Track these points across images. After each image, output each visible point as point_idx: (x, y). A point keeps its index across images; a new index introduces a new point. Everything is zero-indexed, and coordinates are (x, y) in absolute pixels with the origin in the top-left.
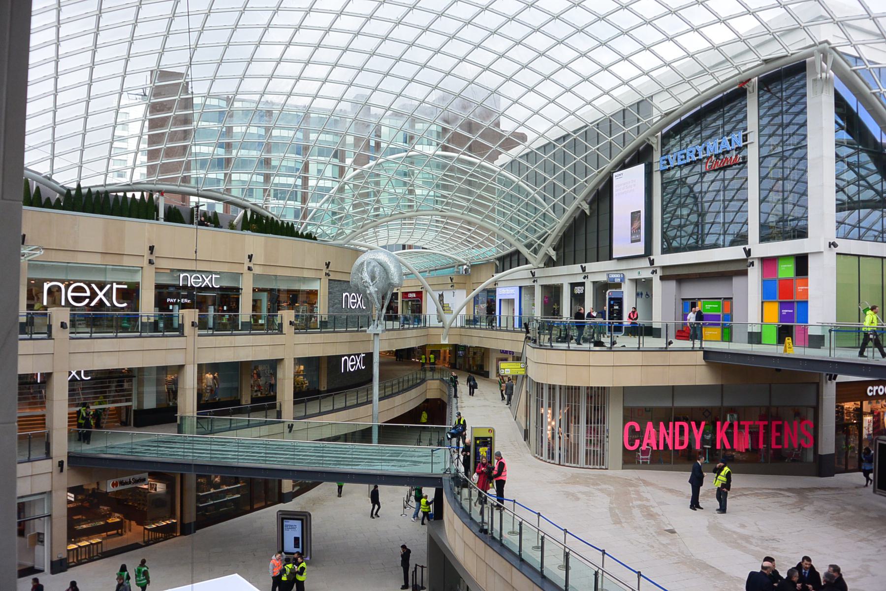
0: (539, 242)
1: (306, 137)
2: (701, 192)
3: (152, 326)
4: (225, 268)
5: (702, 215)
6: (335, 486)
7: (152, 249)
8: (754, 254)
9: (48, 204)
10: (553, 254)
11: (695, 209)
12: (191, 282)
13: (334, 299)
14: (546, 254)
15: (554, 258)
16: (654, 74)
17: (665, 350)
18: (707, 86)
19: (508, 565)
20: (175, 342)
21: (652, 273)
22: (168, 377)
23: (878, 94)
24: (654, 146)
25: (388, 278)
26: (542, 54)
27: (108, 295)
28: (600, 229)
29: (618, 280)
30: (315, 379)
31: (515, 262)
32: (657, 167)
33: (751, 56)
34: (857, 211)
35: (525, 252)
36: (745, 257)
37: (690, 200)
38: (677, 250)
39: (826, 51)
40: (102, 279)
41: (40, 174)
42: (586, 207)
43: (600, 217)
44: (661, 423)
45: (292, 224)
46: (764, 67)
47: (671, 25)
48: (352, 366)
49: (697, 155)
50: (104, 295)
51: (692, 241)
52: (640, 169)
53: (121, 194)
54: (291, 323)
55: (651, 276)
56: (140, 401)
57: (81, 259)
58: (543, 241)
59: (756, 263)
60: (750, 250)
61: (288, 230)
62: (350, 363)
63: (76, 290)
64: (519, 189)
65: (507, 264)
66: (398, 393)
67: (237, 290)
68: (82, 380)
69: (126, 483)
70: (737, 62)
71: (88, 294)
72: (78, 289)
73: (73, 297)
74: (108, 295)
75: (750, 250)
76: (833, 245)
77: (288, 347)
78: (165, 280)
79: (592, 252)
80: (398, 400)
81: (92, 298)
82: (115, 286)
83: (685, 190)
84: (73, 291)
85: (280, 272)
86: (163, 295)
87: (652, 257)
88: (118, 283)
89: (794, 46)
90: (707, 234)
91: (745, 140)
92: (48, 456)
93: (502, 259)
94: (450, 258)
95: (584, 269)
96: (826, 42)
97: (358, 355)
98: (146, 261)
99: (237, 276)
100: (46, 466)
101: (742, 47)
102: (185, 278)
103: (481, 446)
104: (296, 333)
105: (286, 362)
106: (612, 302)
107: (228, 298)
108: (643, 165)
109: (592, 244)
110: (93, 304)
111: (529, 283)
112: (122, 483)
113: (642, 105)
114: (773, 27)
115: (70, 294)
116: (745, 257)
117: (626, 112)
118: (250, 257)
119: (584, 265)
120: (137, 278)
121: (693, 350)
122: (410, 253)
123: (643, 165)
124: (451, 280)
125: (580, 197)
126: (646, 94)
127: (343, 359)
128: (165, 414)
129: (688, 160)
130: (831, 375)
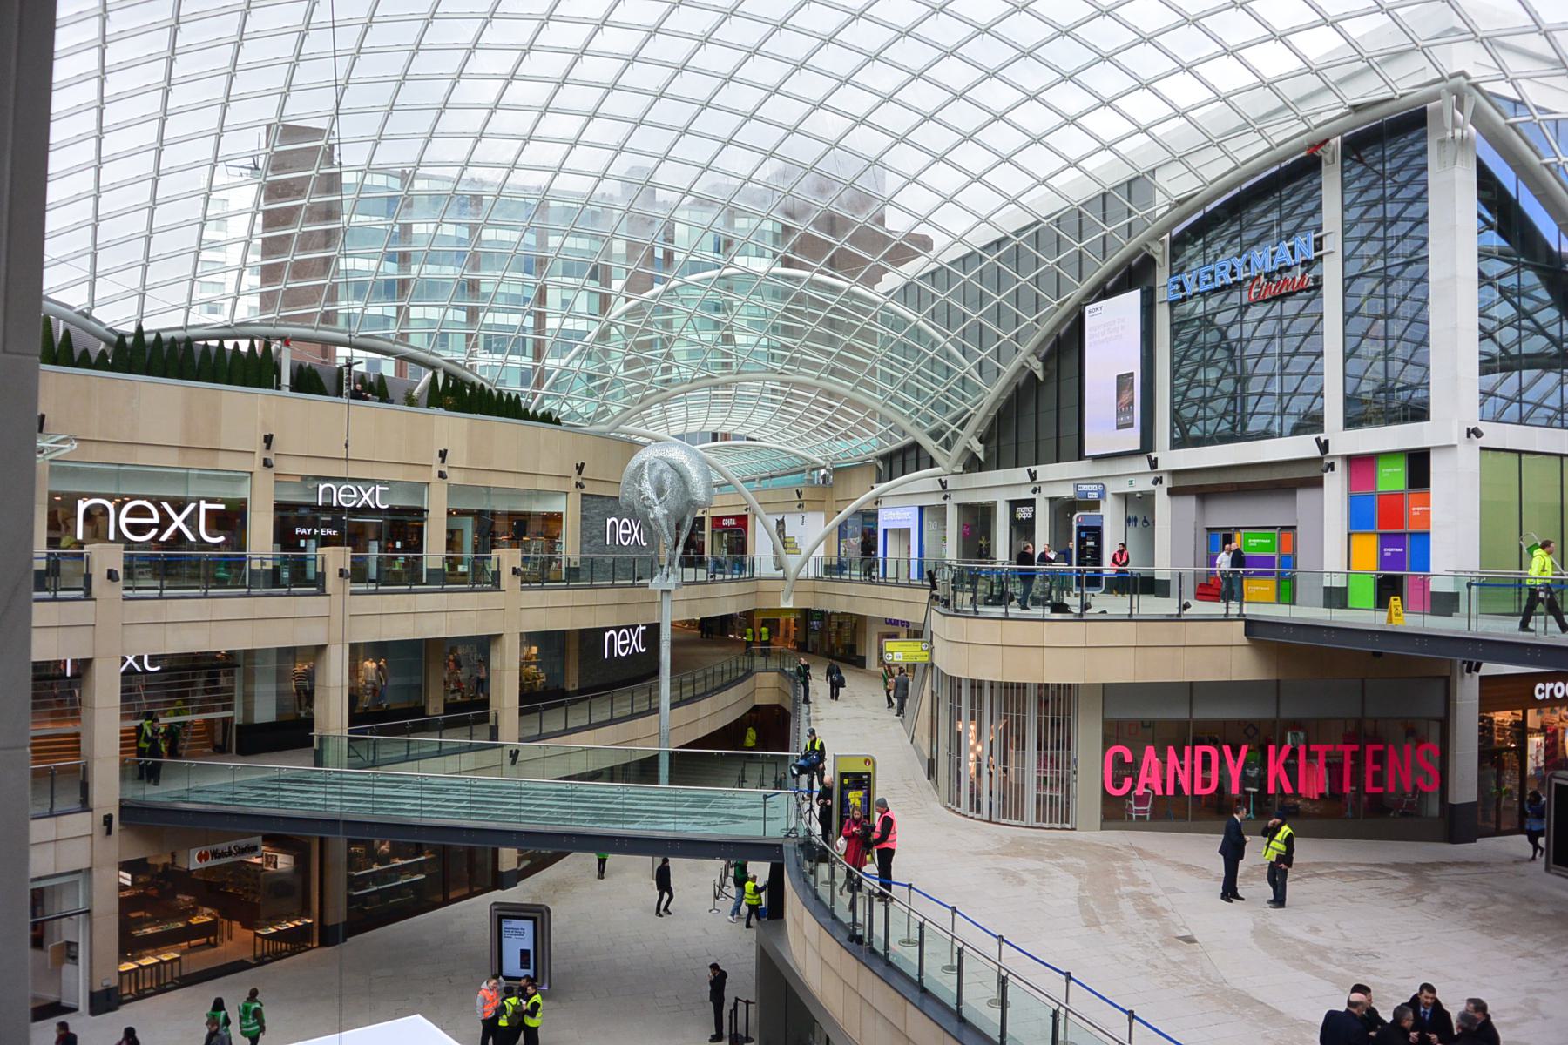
0: (953, 428)
1: (542, 242)
2: (1240, 340)
3: (270, 577)
4: (398, 474)
5: (1242, 380)
6: (592, 859)
7: (268, 439)
8: (1334, 450)
9: (84, 361)
10: (979, 449)
11: (1230, 369)
12: (339, 498)
13: (591, 528)
14: (966, 449)
15: (981, 456)
16: (1157, 131)
17: (1177, 618)
18: (1251, 152)
19: (900, 999)
20: (309, 605)
21: (1155, 483)
22: (297, 667)
23: (1554, 167)
24: (1157, 258)
25: (686, 491)
26: (959, 96)
27: (191, 521)
28: (1062, 404)
29: (1093, 496)
30: (557, 670)
31: (911, 463)
32: (1162, 295)
33: (1329, 100)
34: (1516, 373)
35: (929, 445)
36: (1318, 454)
37: (1220, 354)
38: (1198, 442)
39: (1461, 90)
40: (180, 493)
41: (71, 308)
42: (1037, 366)
43: (1062, 384)
44: (1171, 748)
45: (518, 397)
46: (1352, 119)
47: (1188, 44)
48: (623, 647)
49: (1233, 274)
50: (185, 522)
51: (1224, 426)
52: (1133, 298)
53: (215, 343)
54: (515, 571)
55: (1153, 487)
56: (248, 709)
57: (144, 457)
58: (962, 427)
59: (1338, 465)
60: (1327, 442)
61: (509, 408)
62: (619, 643)
63: (134, 512)
64: (918, 334)
65: (898, 466)
66: (705, 695)
67: (420, 513)
68: (145, 672)
69: (223, 855)
70: (1304, 109)
71: (156, 519)
72: (138, 511)
73: (129, 526)
74: (191, 521)
75: (1327, 442)
76: (1474, 433)
77: (510, 614)
78: (292, 495)
79: (1048, 446)
80: (705, 707)
81: (162, 527)
82: (204, 506)
83: (1213, 337)
84: (129, 515)
85: (495, 481)
86: (288, 521)
87: (1153, 455)
88: (209, 501)
89: (1405, 82)
90: (1252, 414)
91: (1318, 247)
92: (85, 806)
93: (888, 458)
94: (797, 456)
95: (1033, 476)
96: (1463, 73)
97: (634, 627)
98: (258, 462)
99: (419, 488)
100: (81, 823)
101: (1313, 83)
102: (328, 492)
103: (852, 789)
104: (523, 589)
105: (507, 640)
106: (1083, 535)
107: (403, 526)
108: (1138, 292)
109: (1048, 432)
110: (164, 538)
111: (936, 500)
112: (216, 855)
113: (1137, 186)
114: (1369, 48)
115: (124, 520)
116: (1318, 454)
117: (1108, 198)
118: (443, 455)
119: (1033, 468)
120: (243, 492)
121: (1226, 618)
122: (725, 447)
123: (1138, 292)
124: (799, 494)
125: (1026, 348)
126: (1144, 166)
127: (607, 635)
128: (292, 732)
129: (1218, 283)
130: (1470, 664)
